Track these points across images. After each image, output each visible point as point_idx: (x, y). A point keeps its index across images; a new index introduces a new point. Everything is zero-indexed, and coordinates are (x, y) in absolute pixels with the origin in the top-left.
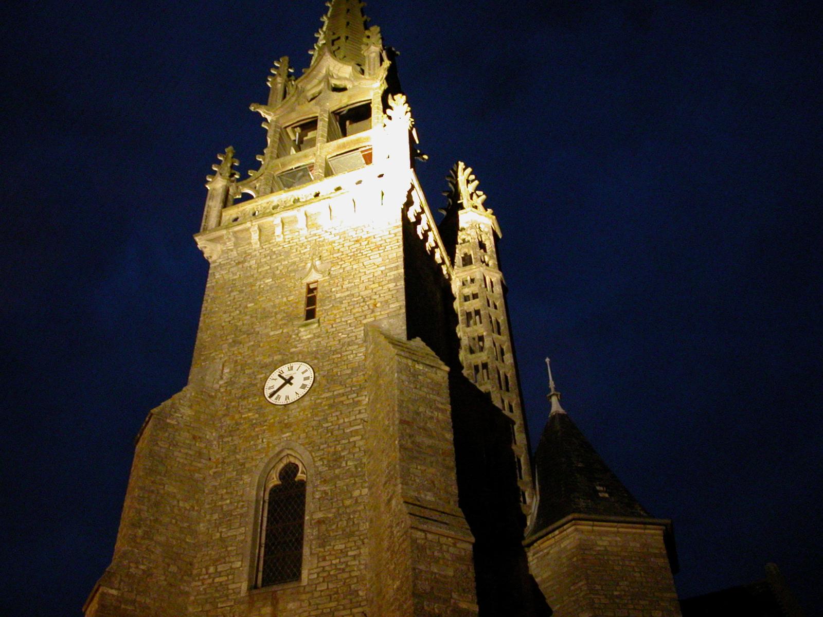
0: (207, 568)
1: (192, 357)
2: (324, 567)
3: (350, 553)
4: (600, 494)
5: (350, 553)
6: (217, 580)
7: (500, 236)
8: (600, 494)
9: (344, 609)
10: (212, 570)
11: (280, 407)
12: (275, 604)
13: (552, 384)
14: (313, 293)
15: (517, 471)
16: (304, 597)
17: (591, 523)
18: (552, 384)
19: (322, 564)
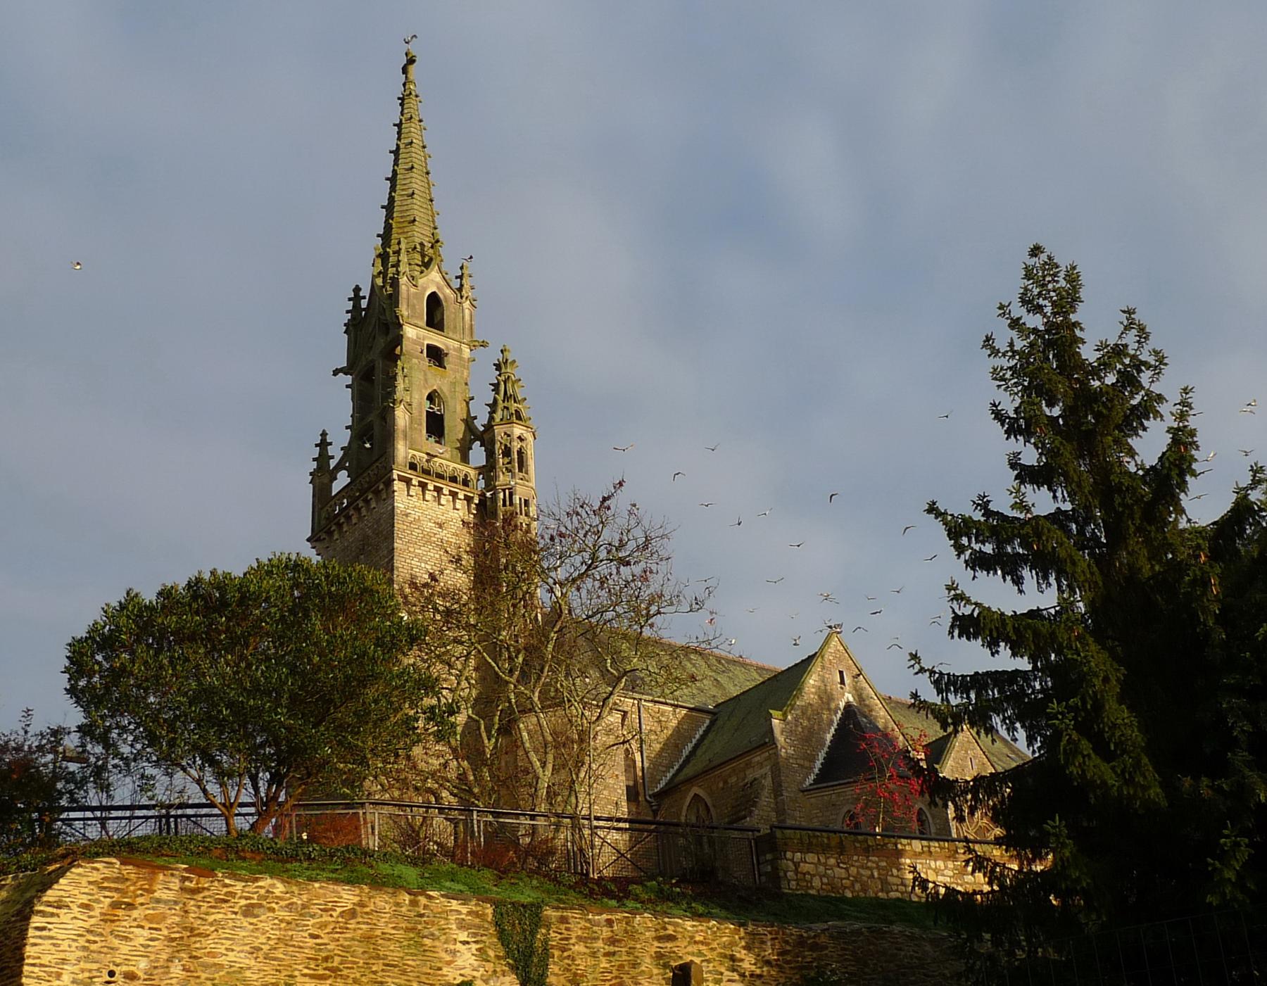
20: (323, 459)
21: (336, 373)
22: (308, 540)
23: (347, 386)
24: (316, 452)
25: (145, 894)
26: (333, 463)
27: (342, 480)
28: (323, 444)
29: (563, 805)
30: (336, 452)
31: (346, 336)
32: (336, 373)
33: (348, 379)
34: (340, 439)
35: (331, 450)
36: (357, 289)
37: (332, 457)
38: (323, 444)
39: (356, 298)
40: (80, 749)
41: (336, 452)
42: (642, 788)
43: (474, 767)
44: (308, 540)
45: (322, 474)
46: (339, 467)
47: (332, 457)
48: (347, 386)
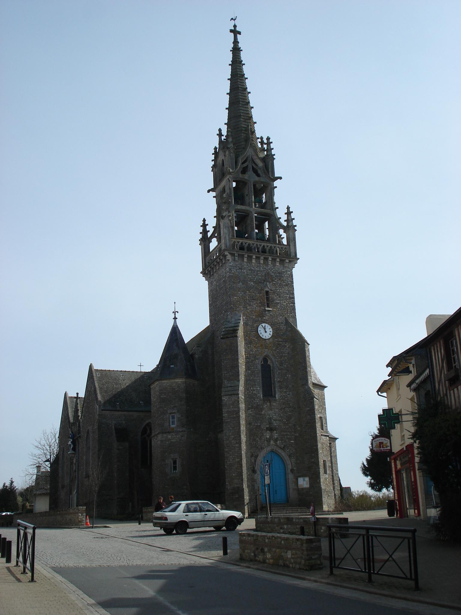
0: (250, 388)
1: (128, 598)
2: (281, 395)
3: (287, 393)
4: (456, 389)
5: (287, 393)
6: (254, 392)
7: (428, 374)
8: (456, 389)
9: (287, 408)
10: (252, 389)
11: (75, 415)
12: (270, 403)
13: (9, 513)
14: (348, 531)
15: (420, 345)
16: (277, 402)
17: (287, 475)
18: (9, 513)
19: (281, 394)
20: (205, 232)
21: (209, 191)
22: (201, 273)
23: (214, 197)
24: (201, 229)
25: (221, 244)
26: (209, 234)
27: (214, 244)
28: (204, 225)
29: (98, 559)
30: (210, 229)
31: (212, 172)
32: (209, 191)
33: (214, 194)
34: (212, 223)
35: (208, 228)
36: (220, 130)
37: (209, 231)
38: (204, 225)
39: (220, 135)
40: (262, 281)
41: (210, 229)
42: (151, 532)
43: (335, 451)
44: (201, 273)
45: (205, 240)
46: (213, 236)
47: (209, 231)
48: (214, 197)
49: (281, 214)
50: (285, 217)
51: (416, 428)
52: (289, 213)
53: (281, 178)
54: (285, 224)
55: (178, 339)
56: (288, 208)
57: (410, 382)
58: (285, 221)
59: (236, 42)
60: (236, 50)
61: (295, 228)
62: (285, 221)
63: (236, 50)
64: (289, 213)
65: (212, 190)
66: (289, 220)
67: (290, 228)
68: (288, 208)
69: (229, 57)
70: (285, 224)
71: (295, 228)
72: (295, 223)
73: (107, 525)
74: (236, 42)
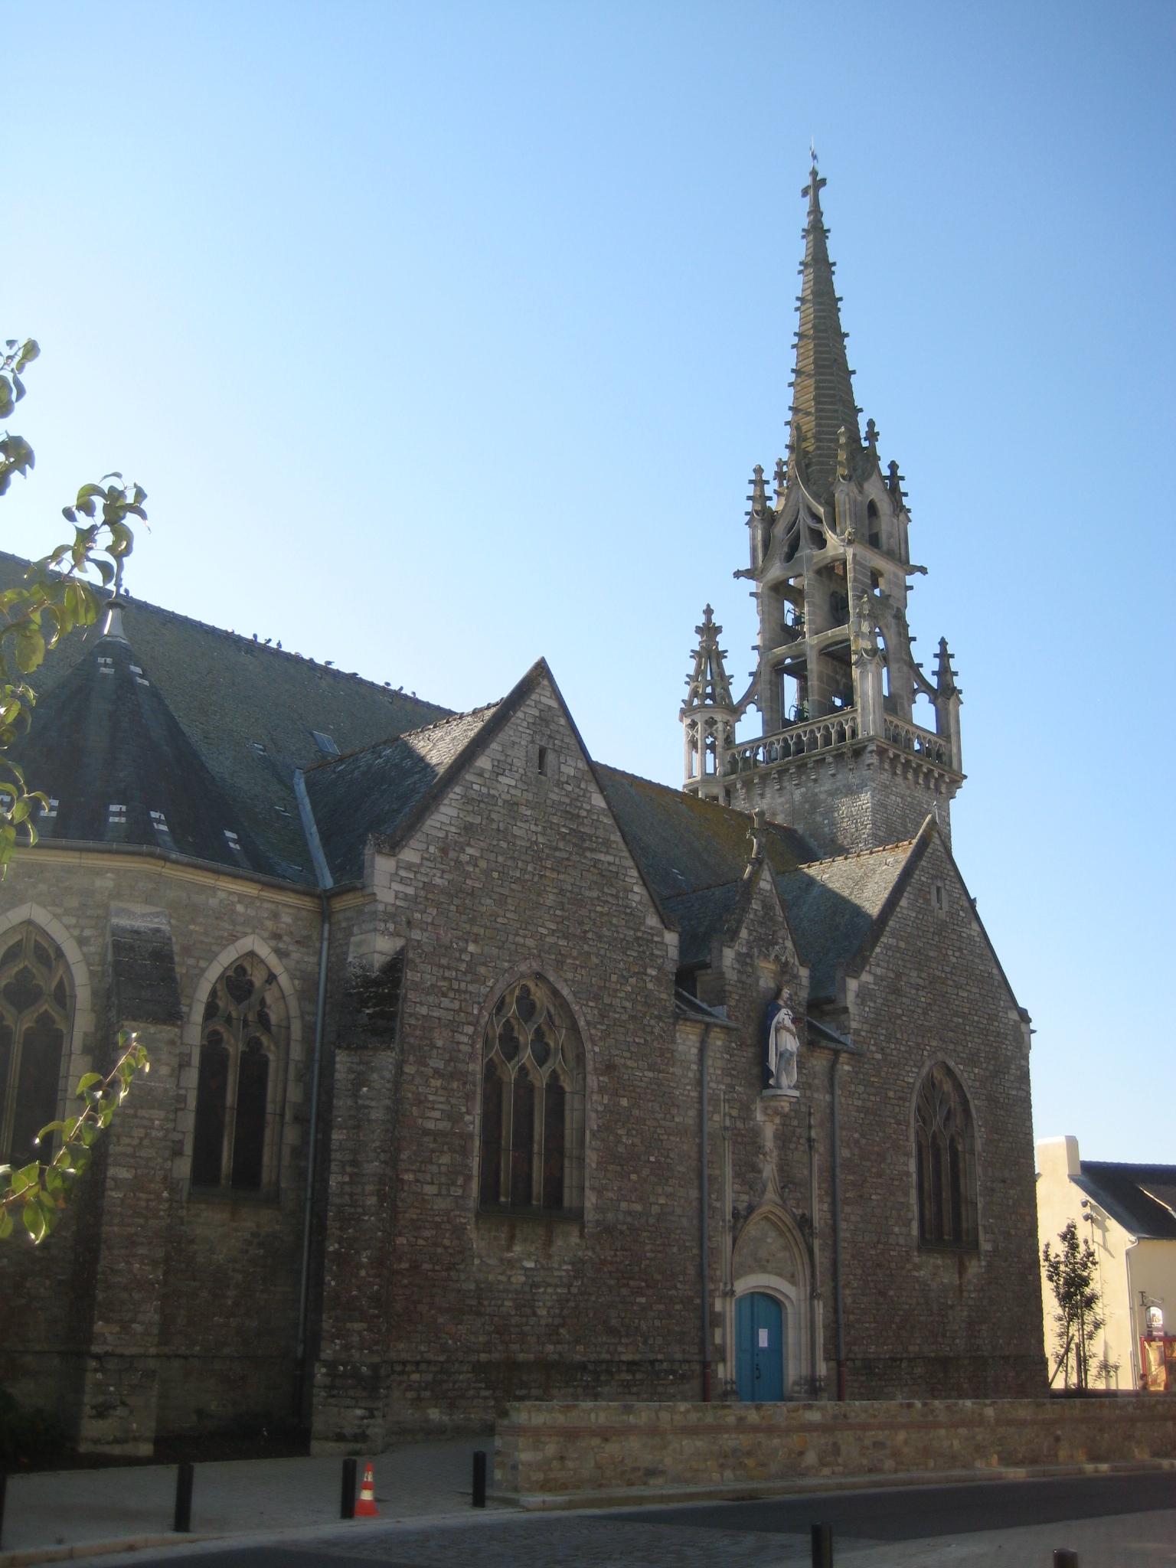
33: (752, 585)
38: (710, 655)
49: (924, 654)
50: (935, 664)
51: (874, 918)
52: (944, 656)
53: (923, 570)
54: (933, 681)
55: (176, 948)
56: (943, 643)
57: (325, 854)
58: (934, 673)
59: (816, 211)
60: (817, 232)
61: (833, 269)
62: (934, 673)
63: (817, 232)
64: (944, 656)
65: (749, 574)
66: (945, 673)
67: (945, 694)
68: (943, 643)
69: (800, 250)
70: (933, 681)
71: (833, 269)
72: (958, 682)
73: (731, 1503)
74: (816, 211)
